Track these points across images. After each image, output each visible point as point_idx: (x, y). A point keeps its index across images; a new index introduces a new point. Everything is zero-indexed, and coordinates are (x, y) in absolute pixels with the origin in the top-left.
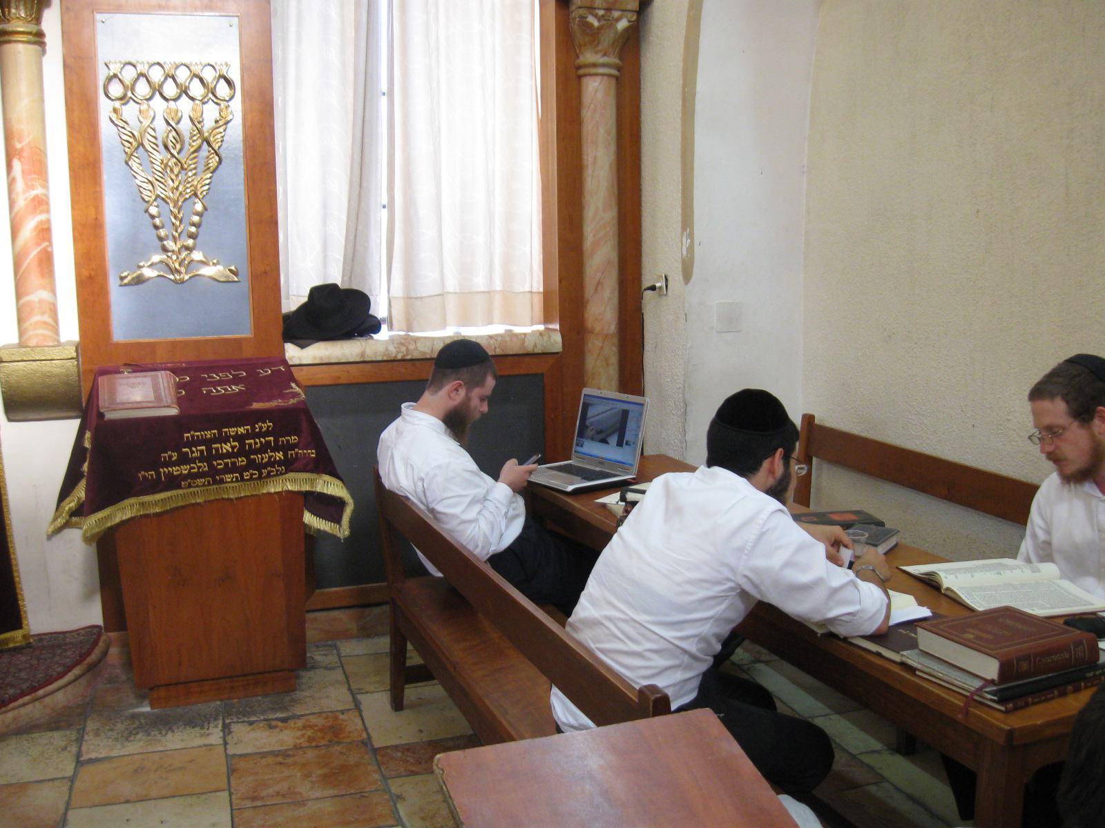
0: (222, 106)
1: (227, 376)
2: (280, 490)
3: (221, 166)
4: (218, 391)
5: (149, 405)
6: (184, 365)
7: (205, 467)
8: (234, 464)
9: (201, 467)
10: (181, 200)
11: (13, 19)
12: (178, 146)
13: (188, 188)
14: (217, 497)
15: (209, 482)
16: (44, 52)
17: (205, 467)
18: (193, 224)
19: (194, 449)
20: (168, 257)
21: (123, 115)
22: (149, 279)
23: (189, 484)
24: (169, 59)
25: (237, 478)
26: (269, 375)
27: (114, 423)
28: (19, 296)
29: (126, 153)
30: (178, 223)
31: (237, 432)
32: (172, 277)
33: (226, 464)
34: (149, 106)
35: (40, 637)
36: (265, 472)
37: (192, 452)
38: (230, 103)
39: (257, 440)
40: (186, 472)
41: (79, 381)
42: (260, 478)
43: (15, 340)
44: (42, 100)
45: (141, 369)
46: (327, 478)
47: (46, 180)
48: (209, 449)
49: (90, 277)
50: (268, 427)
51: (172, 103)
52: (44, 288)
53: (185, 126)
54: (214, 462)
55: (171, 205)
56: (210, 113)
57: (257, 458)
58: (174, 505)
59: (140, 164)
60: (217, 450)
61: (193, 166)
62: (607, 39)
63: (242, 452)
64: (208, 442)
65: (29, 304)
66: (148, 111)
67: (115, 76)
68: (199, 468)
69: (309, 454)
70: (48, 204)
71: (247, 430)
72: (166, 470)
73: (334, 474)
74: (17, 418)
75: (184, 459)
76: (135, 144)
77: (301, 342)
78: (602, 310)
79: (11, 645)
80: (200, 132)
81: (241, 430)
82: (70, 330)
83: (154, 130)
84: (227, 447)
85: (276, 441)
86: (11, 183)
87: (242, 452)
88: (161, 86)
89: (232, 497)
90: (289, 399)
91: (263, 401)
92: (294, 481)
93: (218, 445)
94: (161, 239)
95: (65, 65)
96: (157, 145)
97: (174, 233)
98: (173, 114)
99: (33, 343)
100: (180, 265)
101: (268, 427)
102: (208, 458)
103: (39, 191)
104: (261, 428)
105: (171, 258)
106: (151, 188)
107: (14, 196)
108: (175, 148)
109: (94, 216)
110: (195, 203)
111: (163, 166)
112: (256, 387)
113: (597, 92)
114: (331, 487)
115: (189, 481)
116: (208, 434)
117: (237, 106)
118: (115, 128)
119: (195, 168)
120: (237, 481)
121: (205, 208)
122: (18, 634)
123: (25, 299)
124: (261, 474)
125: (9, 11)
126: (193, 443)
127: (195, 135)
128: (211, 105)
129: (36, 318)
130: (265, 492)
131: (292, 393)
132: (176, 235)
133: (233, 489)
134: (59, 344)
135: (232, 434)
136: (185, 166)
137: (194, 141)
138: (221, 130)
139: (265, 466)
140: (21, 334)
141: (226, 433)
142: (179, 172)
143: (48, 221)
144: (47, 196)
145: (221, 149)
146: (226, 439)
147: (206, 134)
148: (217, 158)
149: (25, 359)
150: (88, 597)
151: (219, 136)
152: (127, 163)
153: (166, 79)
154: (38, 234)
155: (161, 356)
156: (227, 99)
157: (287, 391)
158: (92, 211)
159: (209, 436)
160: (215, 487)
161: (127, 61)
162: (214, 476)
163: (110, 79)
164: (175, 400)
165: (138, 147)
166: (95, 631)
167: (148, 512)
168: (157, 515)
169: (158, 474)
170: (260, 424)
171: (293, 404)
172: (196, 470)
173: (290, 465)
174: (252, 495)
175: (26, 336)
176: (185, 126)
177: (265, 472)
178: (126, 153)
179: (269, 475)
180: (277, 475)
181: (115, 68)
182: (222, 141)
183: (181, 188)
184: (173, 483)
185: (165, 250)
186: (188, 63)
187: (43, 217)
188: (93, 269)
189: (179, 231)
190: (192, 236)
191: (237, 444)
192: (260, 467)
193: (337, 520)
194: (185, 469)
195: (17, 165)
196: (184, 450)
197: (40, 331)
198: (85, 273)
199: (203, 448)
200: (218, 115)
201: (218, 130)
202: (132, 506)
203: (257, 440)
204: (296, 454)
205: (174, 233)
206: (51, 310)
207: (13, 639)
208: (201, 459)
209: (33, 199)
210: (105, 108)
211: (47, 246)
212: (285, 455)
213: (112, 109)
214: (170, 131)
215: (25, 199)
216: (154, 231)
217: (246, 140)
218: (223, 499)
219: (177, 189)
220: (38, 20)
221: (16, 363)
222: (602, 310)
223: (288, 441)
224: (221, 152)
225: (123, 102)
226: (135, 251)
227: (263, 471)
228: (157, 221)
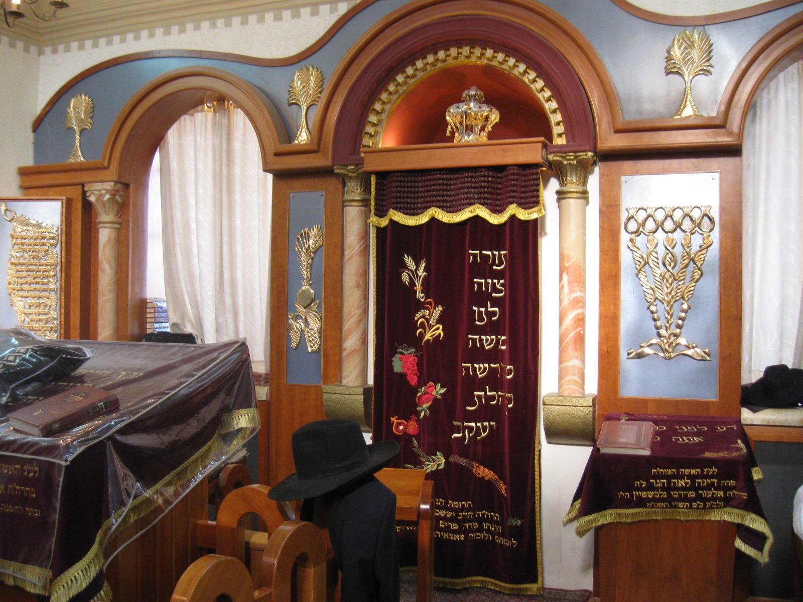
0: (705, 235)
1: (683, 429)
2: (719, 519)
3: (702, 278)
4: (683, 440)
5: (631, 446)
6: (665, 417)
7: (665, 494)
8: (686, 495)
9: (662, 494)
10: (673, 301)
11: (568, 183)
12: (672, 264)
13: (678, 293)
14: (672, 518)
15: (666, 506)
16: (587, 203)
17: (665, 495)
18: (680, 319)
19: (658, 481)
20: (661, 340)
21: (637, 243)
22: (648, 354)
23: (653, 505)
24: (669, 204)
25: (687, 505)
26: (724, 432)
27: (605, 455)
28: (560, 362)
29: (637, 269)
30: (669, 317)
31: (690, 473)
32: (662, 355)
33: (680, 495)
34: (654, 237)
35: (551, 590)
36: (708, 504)
37: (657, 483)
38: (711, 234)
39: (705, 481)
40: (651, 496)
41: (594, 425)
42: (704, 508)
43: (556, 390)
44: (584, 235)
45: (633, 417)
46: (754, 516)
47: (584, 287)
48: (669, 482)
49: (608, 352)
50: (714, 472)
51: (670, 234)
52: (576, 358)
53: (678, 251)
54: (672, 492)
55: (665, 305)
56: (697, 241)
57: (704, 493)
58: (640, 519)
59: (646, 276)
60: (675, 483)
61: (682, 278)
63: (692, 488)
64: (668, 478)
65: (566, 367)
66: (653, 240)
67: (632, 217)
68: (660, 495)
69: (742, 495)
70: (584, 303)
71: (698, 472)
72: (637, 493)
73: (760, 513)
74: (554, 442)
75: (650, 487)
76: (643, 263)
77: (753, 407)
79: (529, 593)
80: (688, 254)
81: (693, 472)
82: (592, 387)
83: (656, 253)
84: (681, 483)
85: (719, 483)
86: (561, 288)
87: (692, 488)
88: (663, 223)
89: (682, 519)
90: (732, 453)
91: (713, 452)
92: (730, 514)
93: (676, 481)
94: (657, 328)
95: (601, 211)
96: (658, 264)
97: (666, 324)
98: (670, 242)
99: (566, 394)
100: (669, 347)
101: (714, 472)
102: (668, 489)
103: (578, 294)
104: (708, 472)
105: (663, 342)
106: (652, 292)
107: (562, 297)
108: (670, 265)
109: (613, 311)
110: (682, 304)
111: (661, 278)
112: (713, 439)
114: (757, 524)
115: (652, 503)
116: (669, 472)
117: (715, 236)
118: (631, 252)
119: (684, 279)
120: (687, 508)
121: (689, 308)
122: (534, 587)
123: (564, 365)
124: (705, 505)
125: (566, 178)
126: (658, 477)
127: (685, 256)
128: (696, 236)
129: (570, 378)
130: (707, 519)
131: (737, 447)
132: (668, 325)
133: (683, 513)
134: (584, 396)
135: (686, 473)
136: (677, 278)
137: (684, 260)
138: (704, 252)
139: (709, 500)
140: (560, 387)
141: (682, 472)
142: (672, 282)
143: (583, 314)
144: (584, 298)
145: (703, 266)
146: (682, 477)
147: (692, 256)
148: (700, 272)
149: (560, 404)
150: (585, 569)
151: (702, 256)
152: (637, 275)
153: (666, 218)
154: (575, 323)
155: (651, 409)
156: (708, 230)
157: (733, 446)
158: (612, 308)
159: (669, 473)
160: (671, 510)
161: (641, 206)
162: (671, 502)
163: (629, 219)
164: (649, 445)
165: (645, 265)
166: (586, 594)
167: (622, 521)
168: (626, 523)
169: (632, 495)
170: (707, 469)
171: (735, 457)
172: (658, 496)
173: (727, 502)
174: (698, 520)
175: (563, 389)
176: (678, 251)
177: (708, 504)
178: (637, 269)
179: (711, 507)
180: (717, 508)
181: (632, 212)
182: (704, 260)
183: (673, 293)
184: (641, 503)
185: (659, 335)
186: (682, 206)
187: (580, 311)
188: (609, 347)
189: (670, 322)
190: (679, 327)
191: (689, 481)
192: (705, 500)
193: (760, 548)
194: (650, 494)
195: (565, 277)
196: (651, 481)
197: (572, 387)
198: (605, 349)
199: (665, 481)
200: (702, 242)
201: (701, 253)
202: (611, 514)
203: (705, 481)
204: (734, 494)
205: (666, 324)
206: (579, 372)
207: (531, 589)
208: (663, 489)
209: (574, 299)
210: (625, 237)
211: (581, 330)
212: (725, 493)
213: (629, 239)
214: (668, 254)
215: (569, 299)
216: (653, 323)
217: (721, 259)
218: (677, 520)
219: (670, 293)
220: (584, 182)
221: (553, 407)
223: (728, 484)
224: (703, 268)
225: (637, 234)
226: (639, 335)
227: (707, 504)
228: (656, 315)
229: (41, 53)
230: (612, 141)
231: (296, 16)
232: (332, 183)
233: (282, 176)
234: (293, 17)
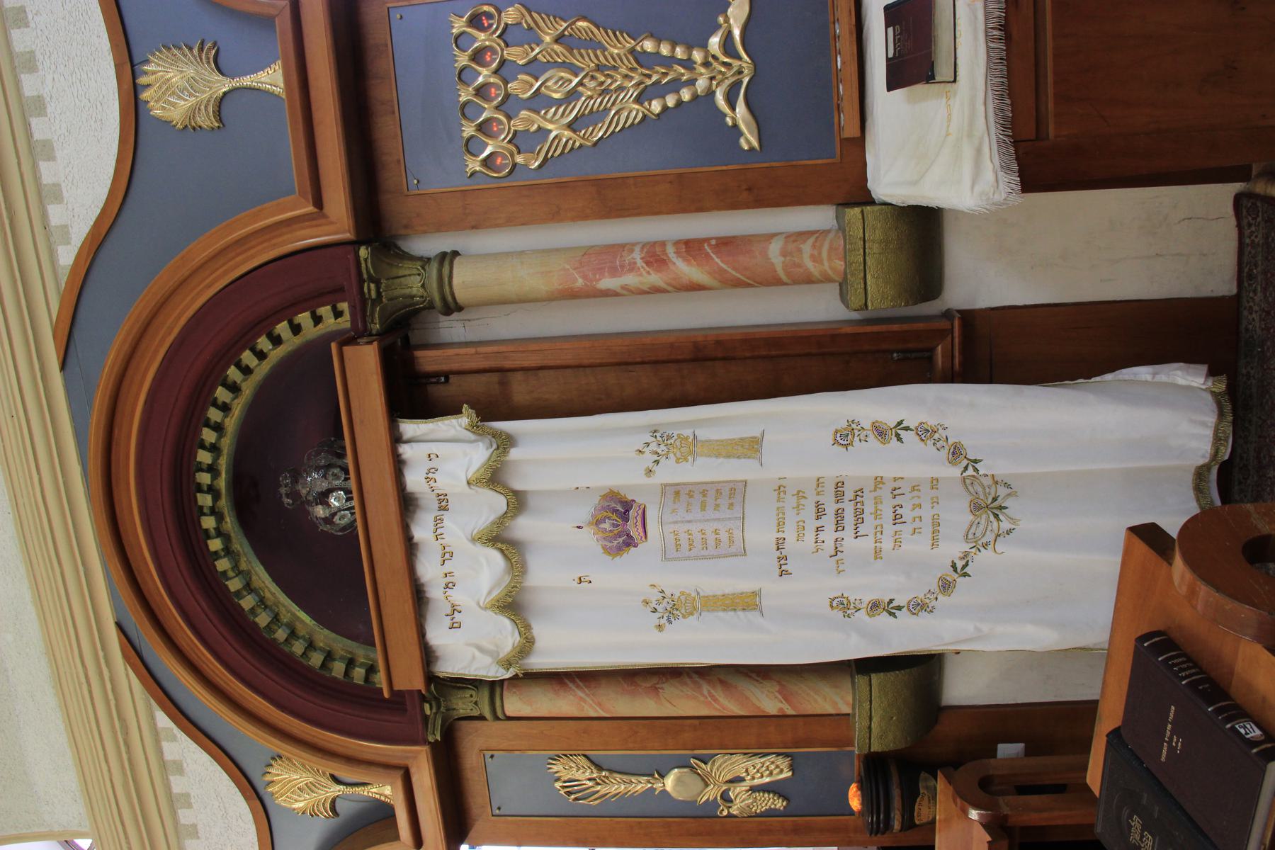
103: (637, 256)
140: (827, 279)
220: (426, 261)
230: (338, 221)
231: (186, 800)
234: (189, 806)
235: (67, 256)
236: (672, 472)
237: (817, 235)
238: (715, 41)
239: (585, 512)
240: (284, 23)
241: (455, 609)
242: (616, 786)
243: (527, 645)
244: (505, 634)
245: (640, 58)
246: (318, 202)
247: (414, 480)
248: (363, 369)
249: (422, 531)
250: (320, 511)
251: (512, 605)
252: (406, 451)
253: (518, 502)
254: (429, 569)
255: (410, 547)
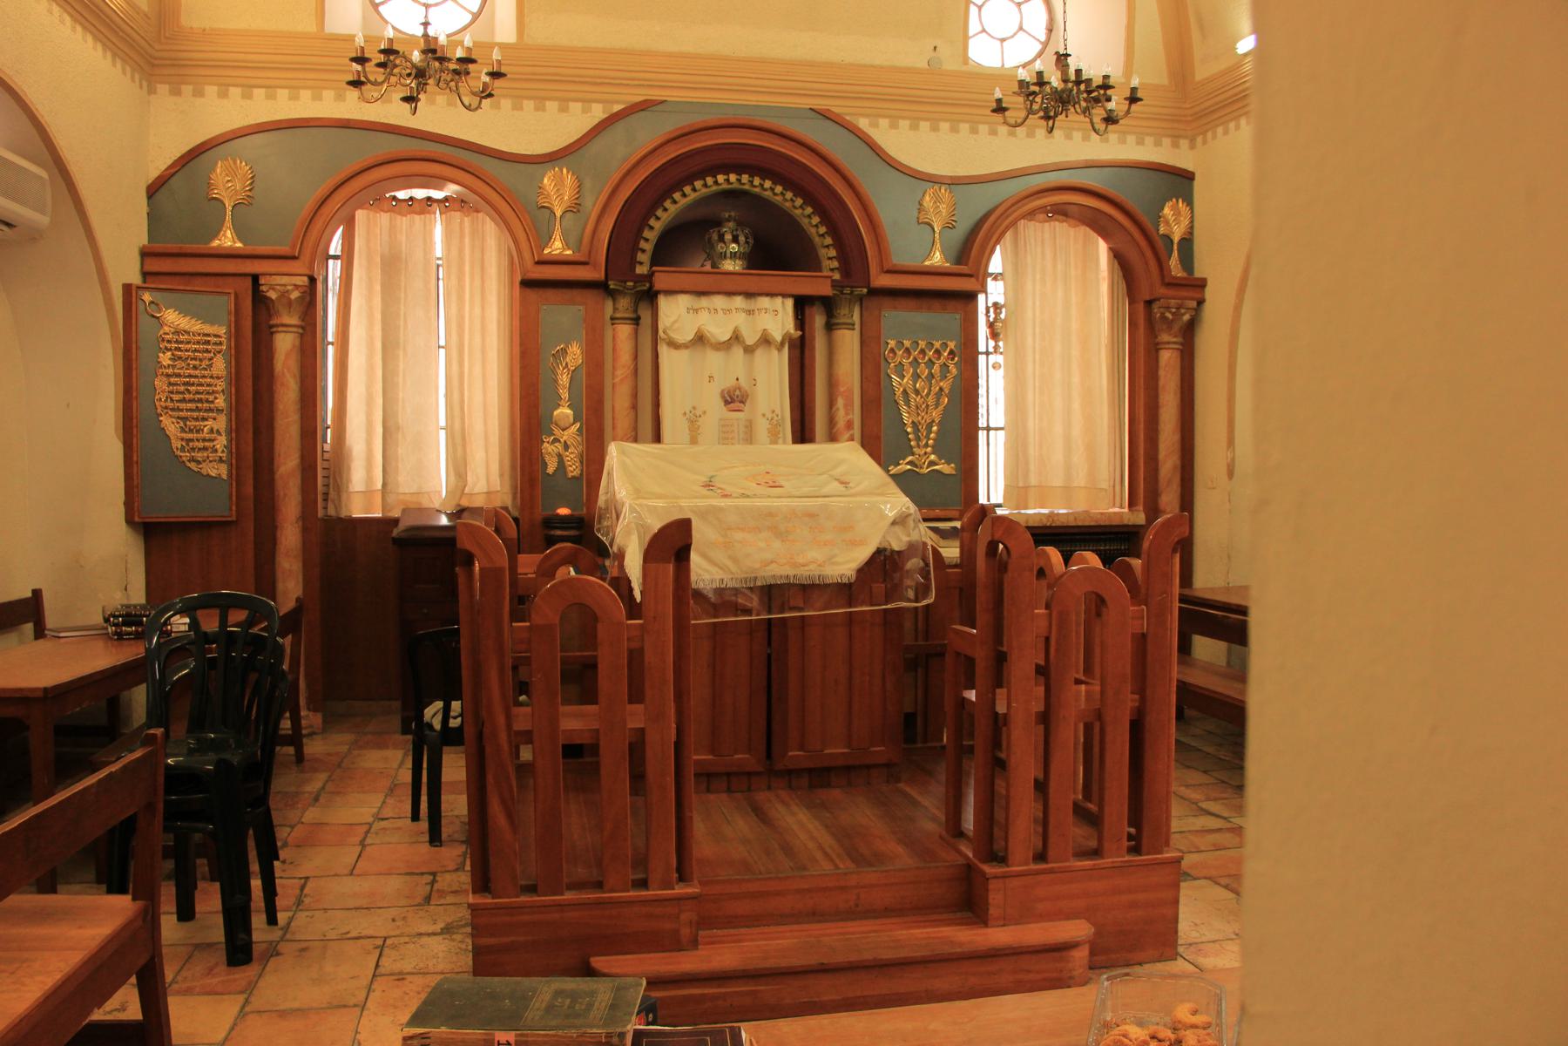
62: (1176, 327)
78: (1169, 499)
113: (1168, 358)
222: (1169, 499)
229: (152, 91)
232: (591, 296)
233: (527, 284)
234: (537, 109)
235: (863, 124)
236: (762, 427)
237: (266, 578)
238: (933, 457)
239: (743, 382)
240: (963, 269)
241: (696, 311)
242: (564, 379)
243: (673, 345)
244: (687, 335)
245: (930, 426)
246: (888, 272)
247: (764, 302)
248: (818, 286)
249: (739, 301)
250: (728, 237)
251: (700, 339)
252: (779, 300)
253: (749, 350)
254: (719, 301)
255: (730, 294)
